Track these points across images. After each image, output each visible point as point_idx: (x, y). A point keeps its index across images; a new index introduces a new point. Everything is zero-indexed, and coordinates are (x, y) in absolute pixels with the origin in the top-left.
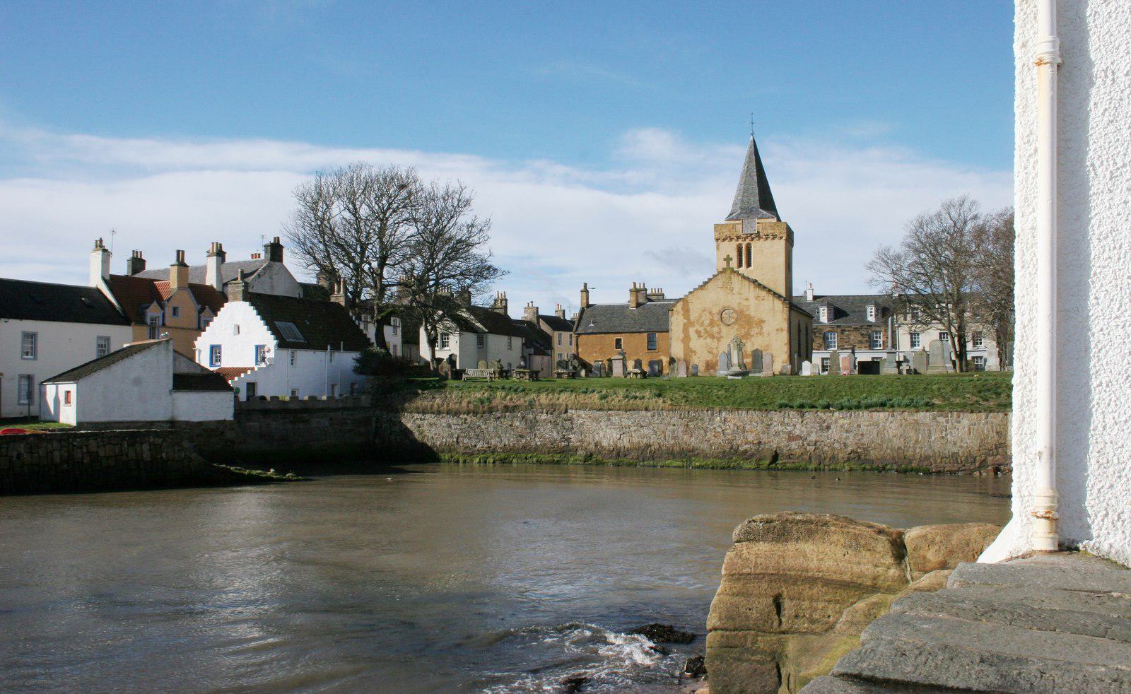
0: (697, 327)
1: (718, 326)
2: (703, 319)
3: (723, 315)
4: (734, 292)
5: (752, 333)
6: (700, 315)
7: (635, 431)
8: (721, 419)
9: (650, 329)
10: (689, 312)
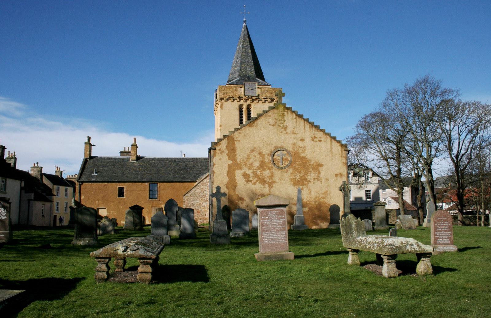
0: (245, 170)
1: (269, 169)
2: (252, 160)
3: (275, 157)
4: (288, 131)
5: (308, 178)
6: (248, 156)
9: (152, 179)
10: (235, 152)
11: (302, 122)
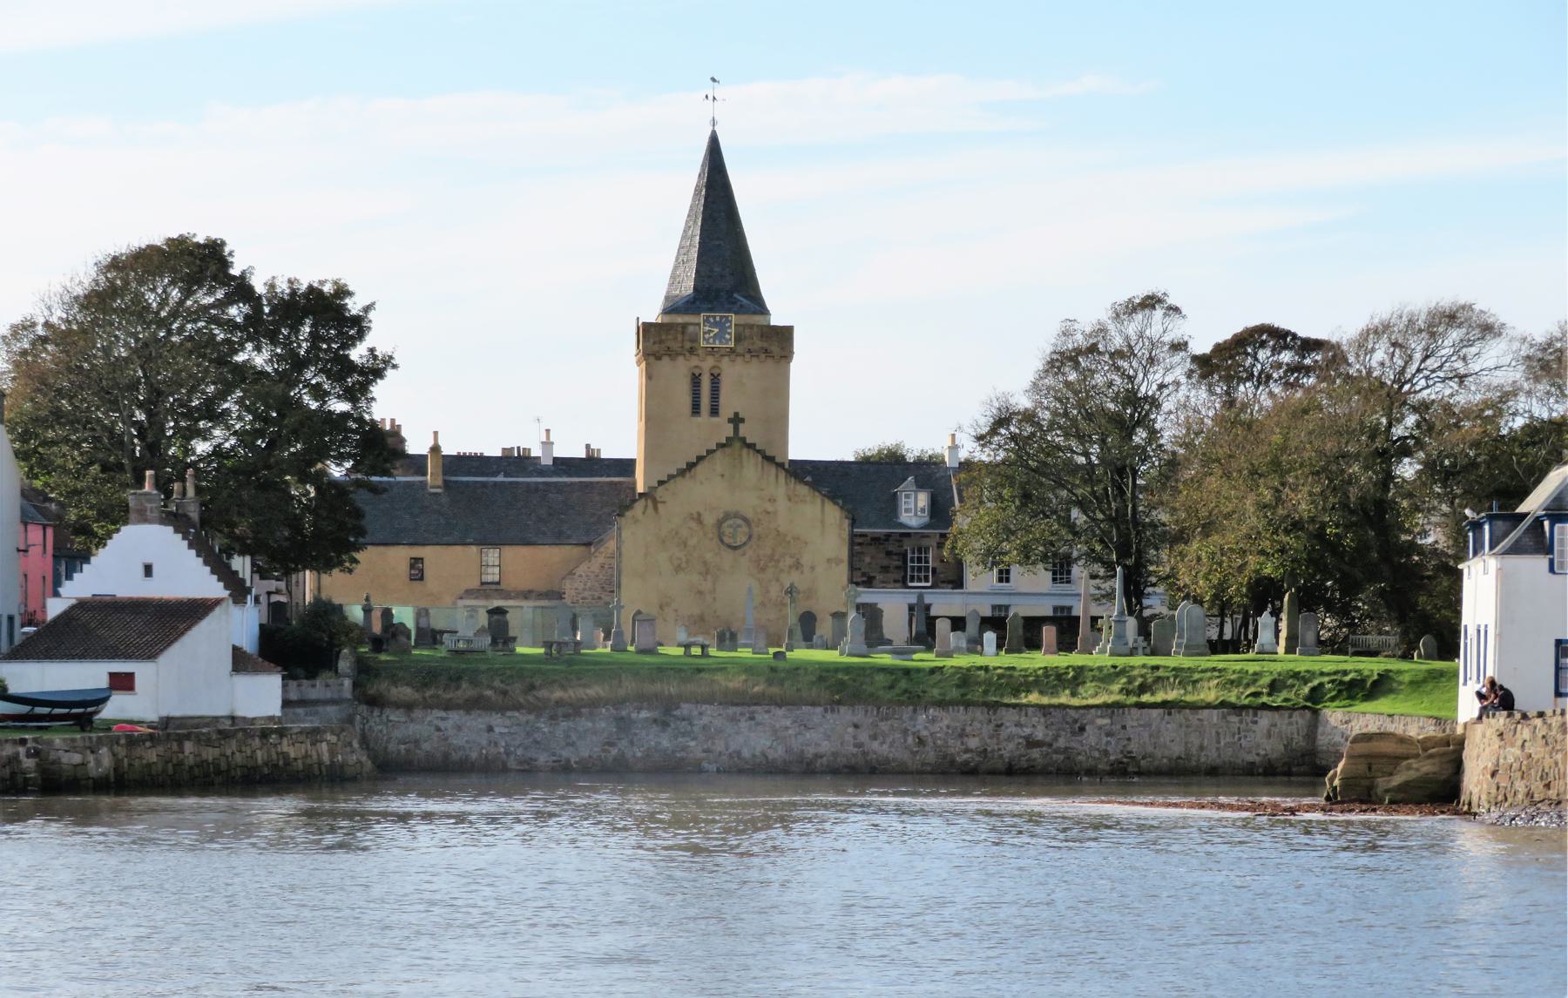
7: (796, 736)
8: (927, 717)
11: (773, 469)
